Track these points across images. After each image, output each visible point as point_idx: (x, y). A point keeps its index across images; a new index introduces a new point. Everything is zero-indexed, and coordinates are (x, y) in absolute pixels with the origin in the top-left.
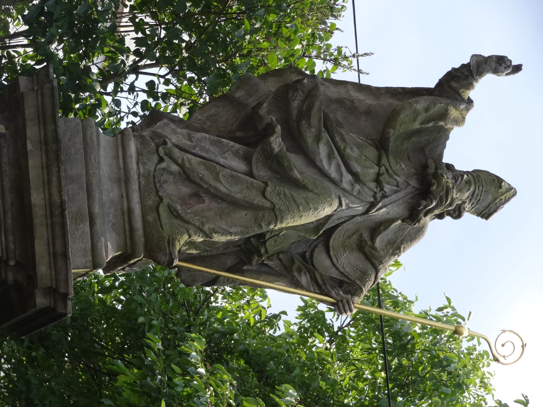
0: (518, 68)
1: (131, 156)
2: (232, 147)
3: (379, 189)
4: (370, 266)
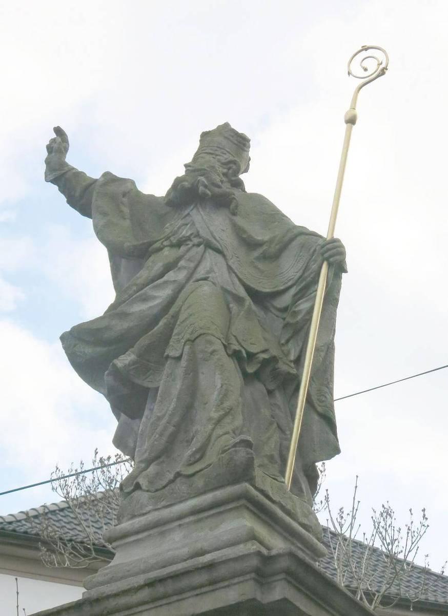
0: (58, 131)
1: (131, 524)
2: (147, 418)
3: (189, 242)
4: (294, 243)
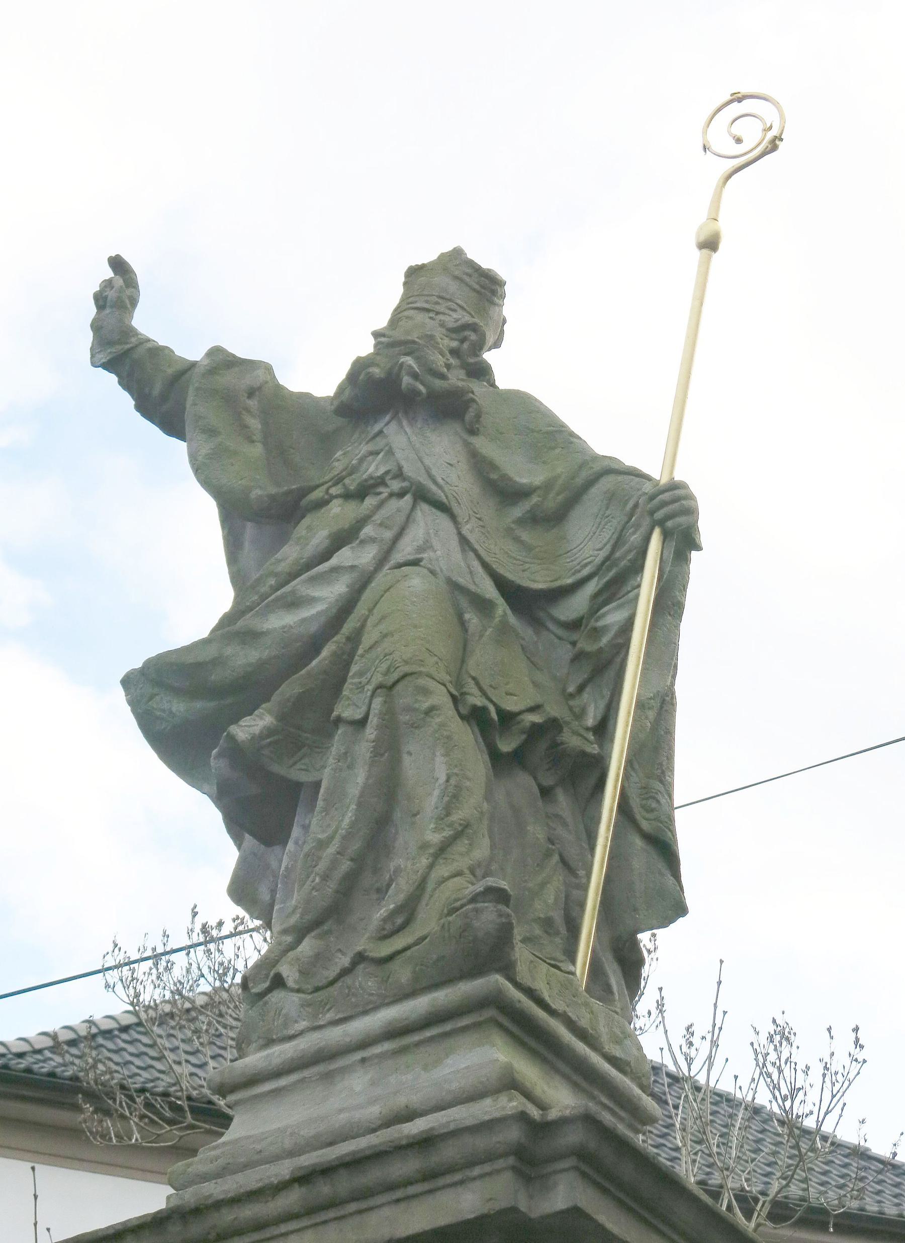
0: (118, 264)
2: (296, 843)
3: (381, 489)
4: (594, 490)
